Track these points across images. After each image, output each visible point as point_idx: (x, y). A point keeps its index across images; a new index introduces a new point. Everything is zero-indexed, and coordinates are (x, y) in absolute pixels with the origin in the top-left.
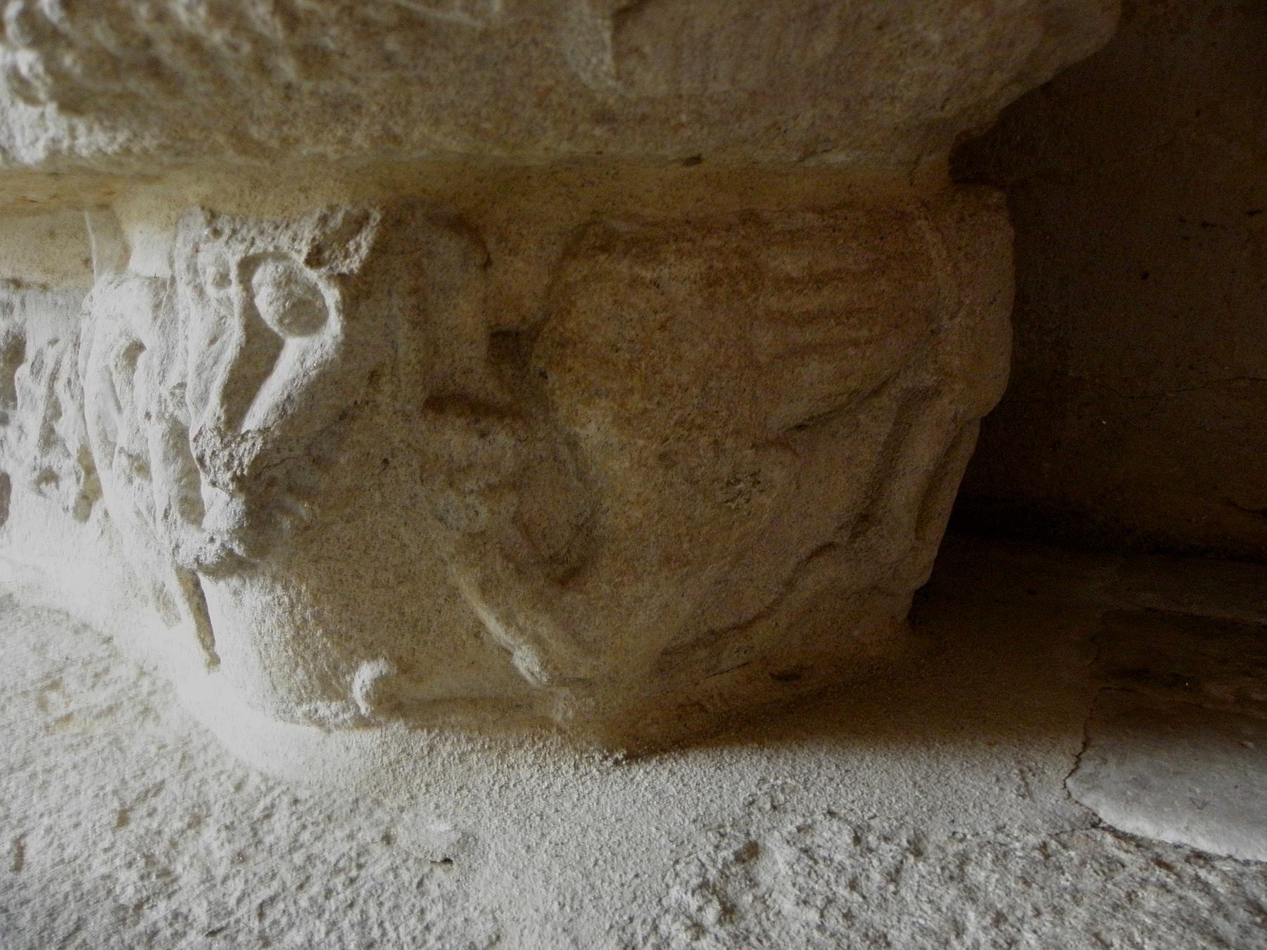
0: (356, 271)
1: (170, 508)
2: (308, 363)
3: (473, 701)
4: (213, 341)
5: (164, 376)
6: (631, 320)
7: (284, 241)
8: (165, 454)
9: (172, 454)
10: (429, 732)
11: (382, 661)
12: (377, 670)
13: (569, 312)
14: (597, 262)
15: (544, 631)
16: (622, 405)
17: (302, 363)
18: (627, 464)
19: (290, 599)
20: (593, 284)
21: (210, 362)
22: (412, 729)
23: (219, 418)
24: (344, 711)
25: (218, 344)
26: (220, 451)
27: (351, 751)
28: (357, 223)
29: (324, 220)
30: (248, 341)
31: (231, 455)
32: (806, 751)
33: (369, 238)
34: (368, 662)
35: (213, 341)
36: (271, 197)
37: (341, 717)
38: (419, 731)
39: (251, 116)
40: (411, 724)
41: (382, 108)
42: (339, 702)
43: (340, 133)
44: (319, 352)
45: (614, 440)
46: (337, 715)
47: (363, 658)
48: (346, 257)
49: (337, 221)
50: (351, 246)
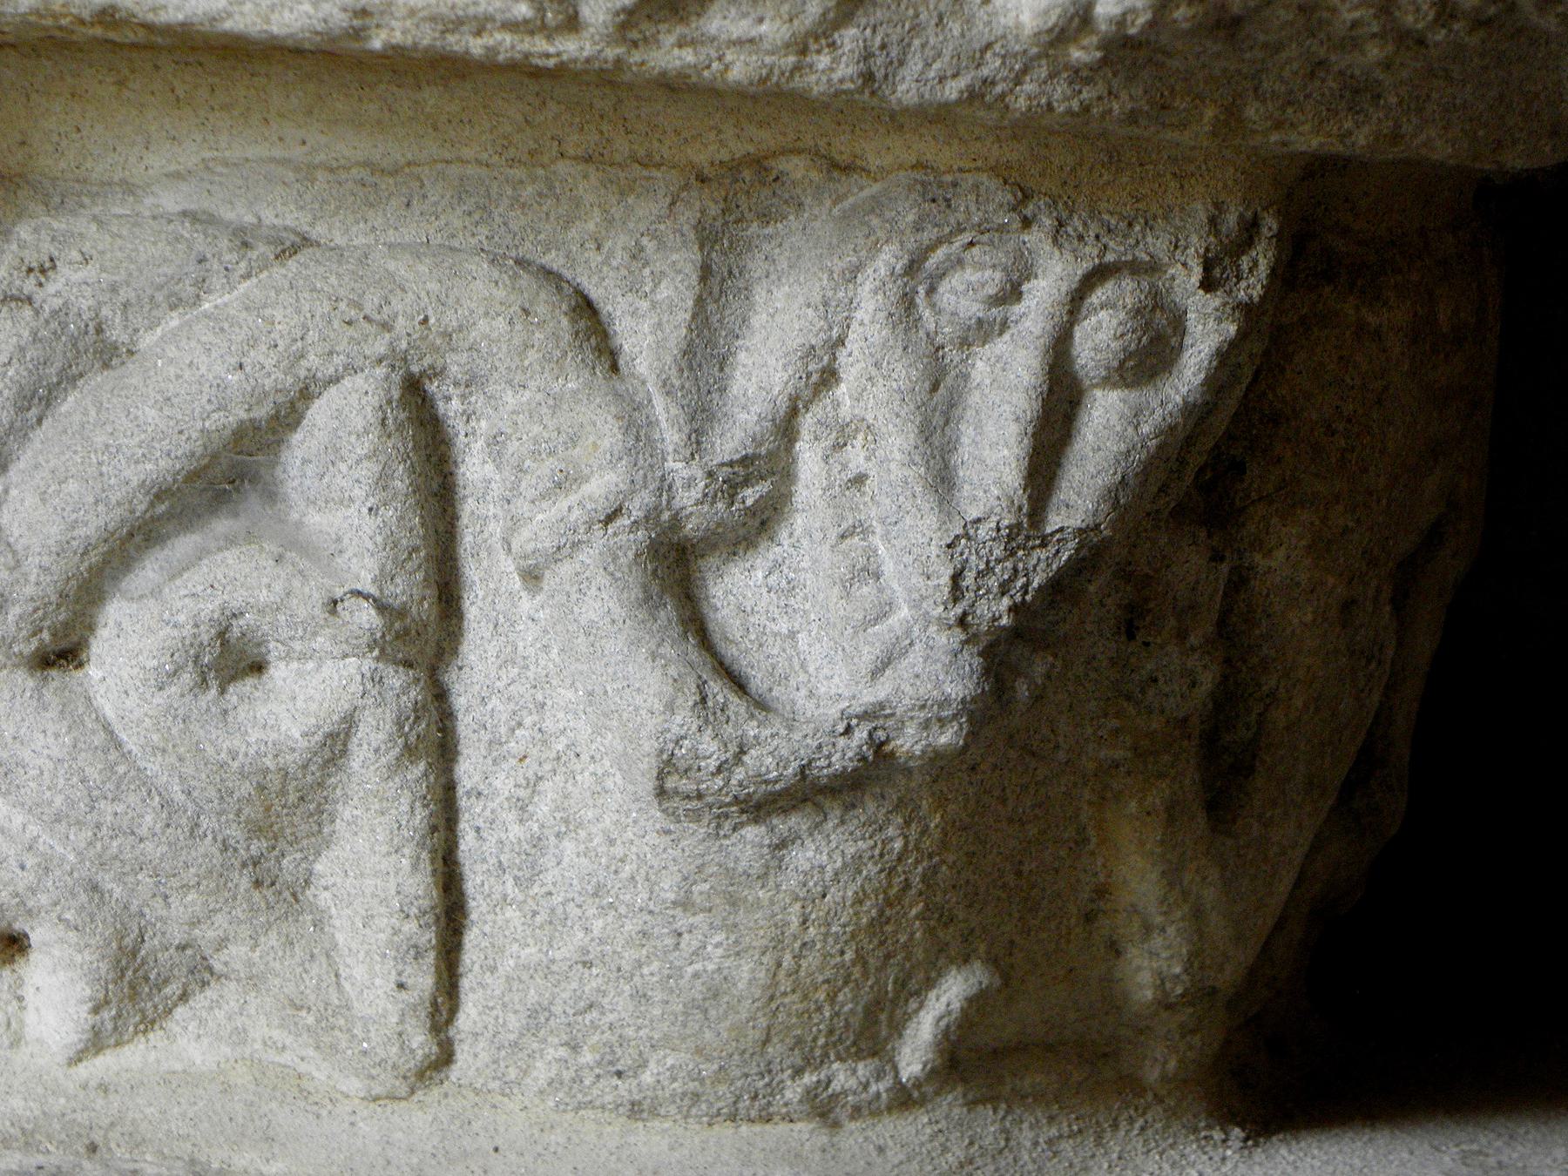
0: (1256, 299)
1: (904, 653)
2: (1145, 429)
3: (1049, 1048)
4: (935, 387)
5: (698, 443)
6: (1353, 387)
7: (1158, 244)
8: (645, 588)
9: (655, 589)
10: (995, 1110)
11: (977, 965)
12: (972, 980)
13: (1282, 370)
14: (1320, 296)
15: (1210, 895)
16: (1324, 520)
17: (1136, 428)
18: (1309, 617)
19: (906, 844)
20: (1315, 329)
21: (938, 420)
22: (971, 1104)
23: (1020, 509)
24: (878, 1079)
25: (942, 390)
26: (998, 561)
27: (889, 1153)
28: (1250, 230)
29: (1213, 222)
30: (1050, 390)
31: (1015, 570)
32: (1426, 1146)
33: (1270, 254)
34: (959, 968)
35: (935, 387)
36: (1125, 179)
37: (873, 1088)
38: (980, 1108)
39: (1256, 90)
40: (970, 1097)
41: (1400, 103)
42: (869, 1061)
43: (1348, 125)
44: (1159, 411)
45: (1303, 577)
46: (866, 1086)
47: (952, 962)
48: (1239, 278)
49: (1231, 220)
50: (1245, 263)
